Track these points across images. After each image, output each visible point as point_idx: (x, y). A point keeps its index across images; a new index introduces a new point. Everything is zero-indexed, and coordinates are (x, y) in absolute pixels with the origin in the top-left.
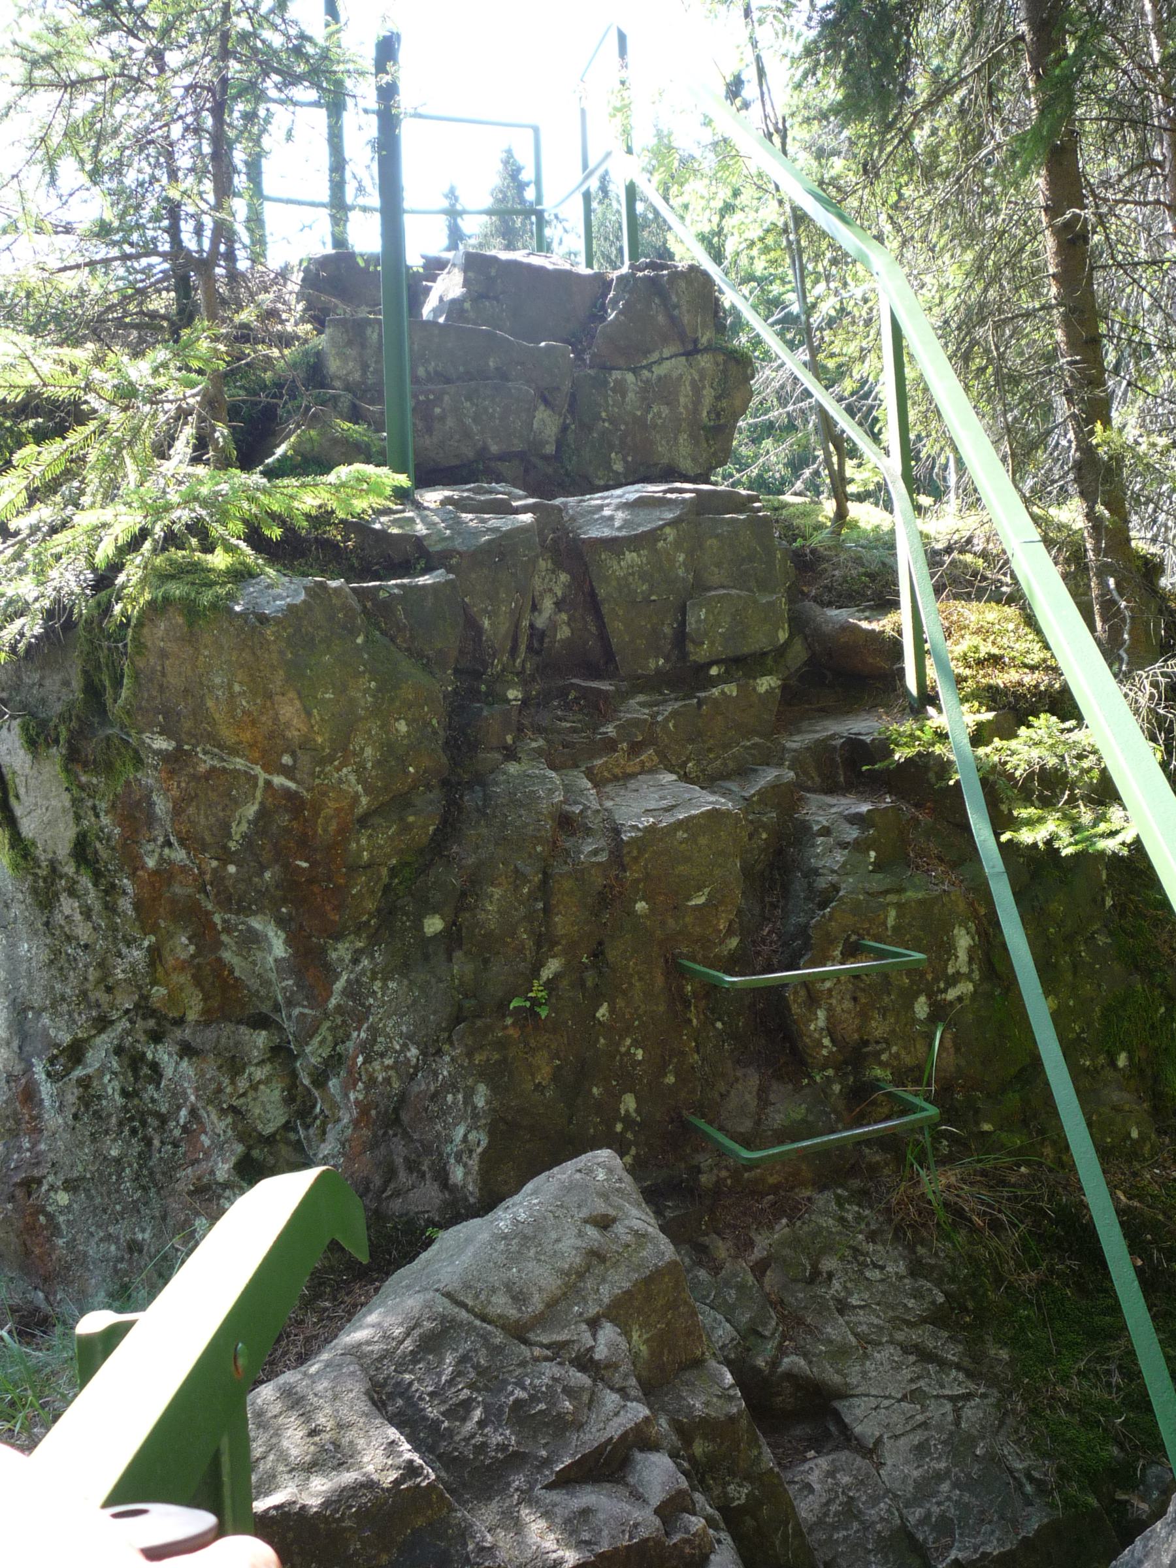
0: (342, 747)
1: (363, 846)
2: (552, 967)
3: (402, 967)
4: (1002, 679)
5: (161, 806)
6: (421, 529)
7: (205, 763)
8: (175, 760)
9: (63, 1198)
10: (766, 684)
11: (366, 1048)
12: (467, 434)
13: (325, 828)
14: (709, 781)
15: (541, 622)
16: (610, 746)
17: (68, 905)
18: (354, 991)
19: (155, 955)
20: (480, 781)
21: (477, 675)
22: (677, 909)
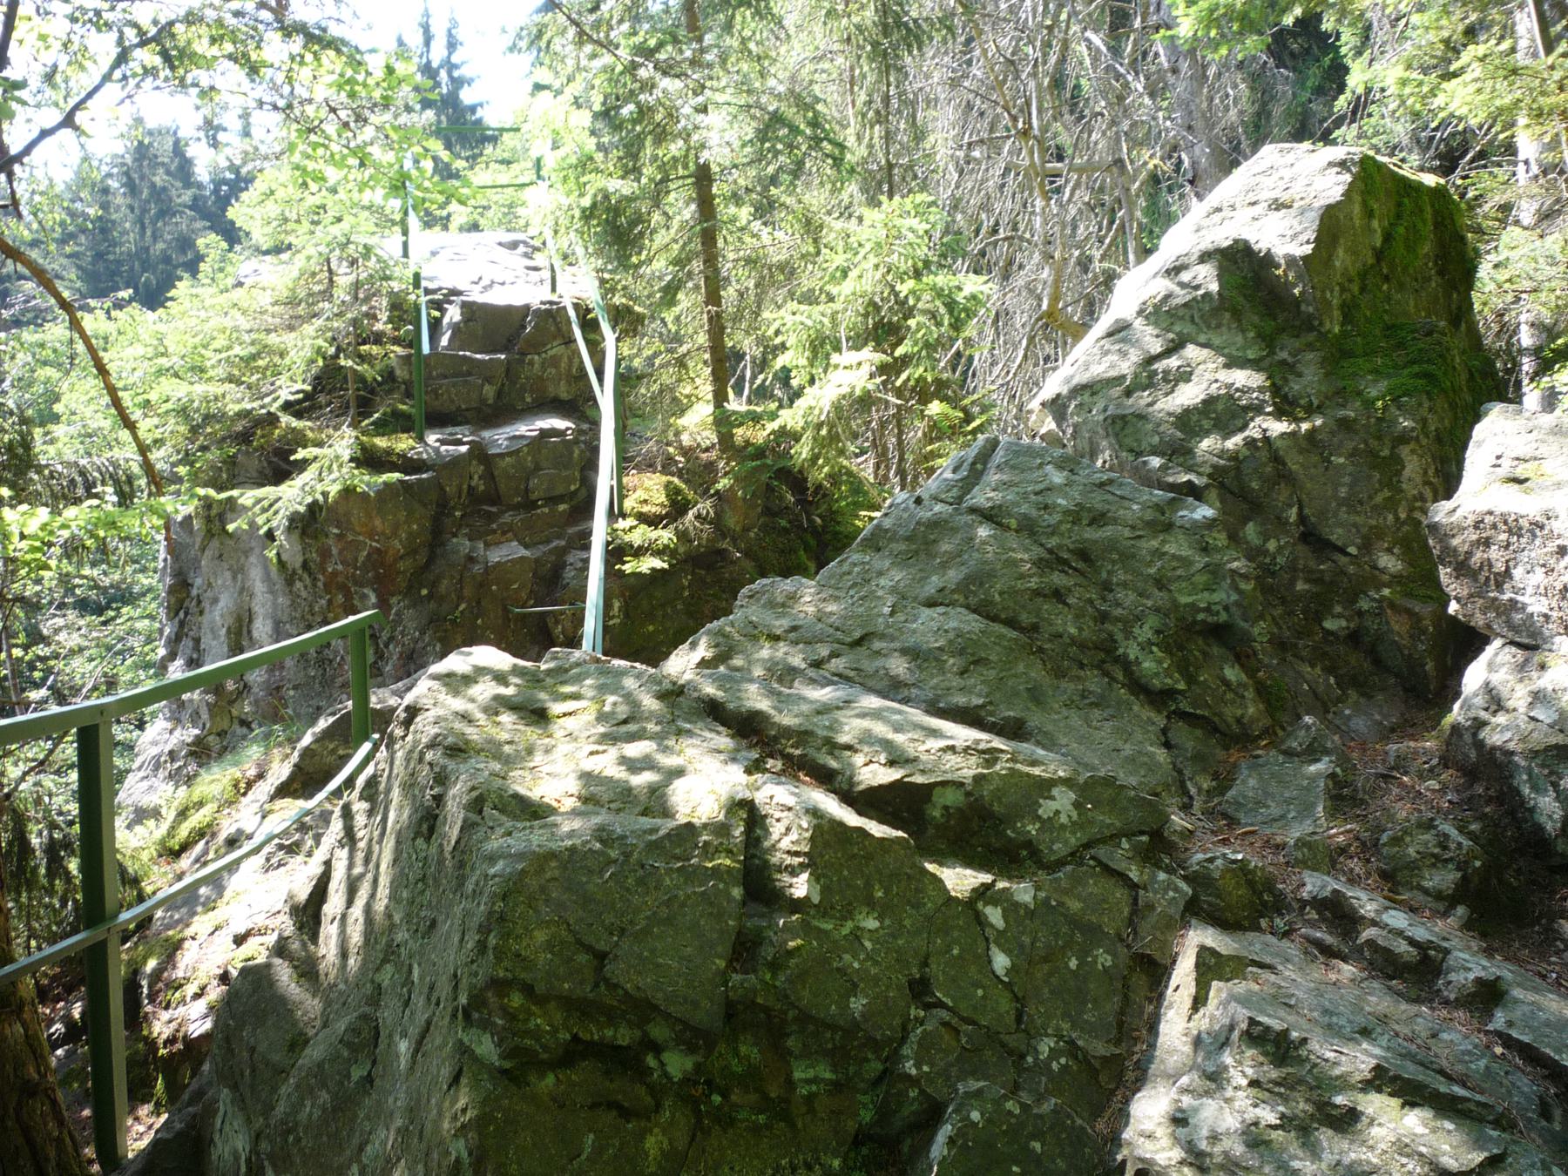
0: (395, 534)
1: (401, 566)
2: (463, 606)
3: (414, 606)
4: (645, 509)
5: (335, 551)
6: (425, 456)
7: (351, 538)
8: (340, 537)
9: (292, 693)
10: (562, 507)
11: (402, 633)
12: (452, 401)
13: (389, 559)
14: (526, 547)
15: (473, 483)
16: (494, 532)
17: (299, 585)
18: (398, 614)
19: (330, 602)
20: (443, 544)
21: (445, 506)
22: (507, 589)
